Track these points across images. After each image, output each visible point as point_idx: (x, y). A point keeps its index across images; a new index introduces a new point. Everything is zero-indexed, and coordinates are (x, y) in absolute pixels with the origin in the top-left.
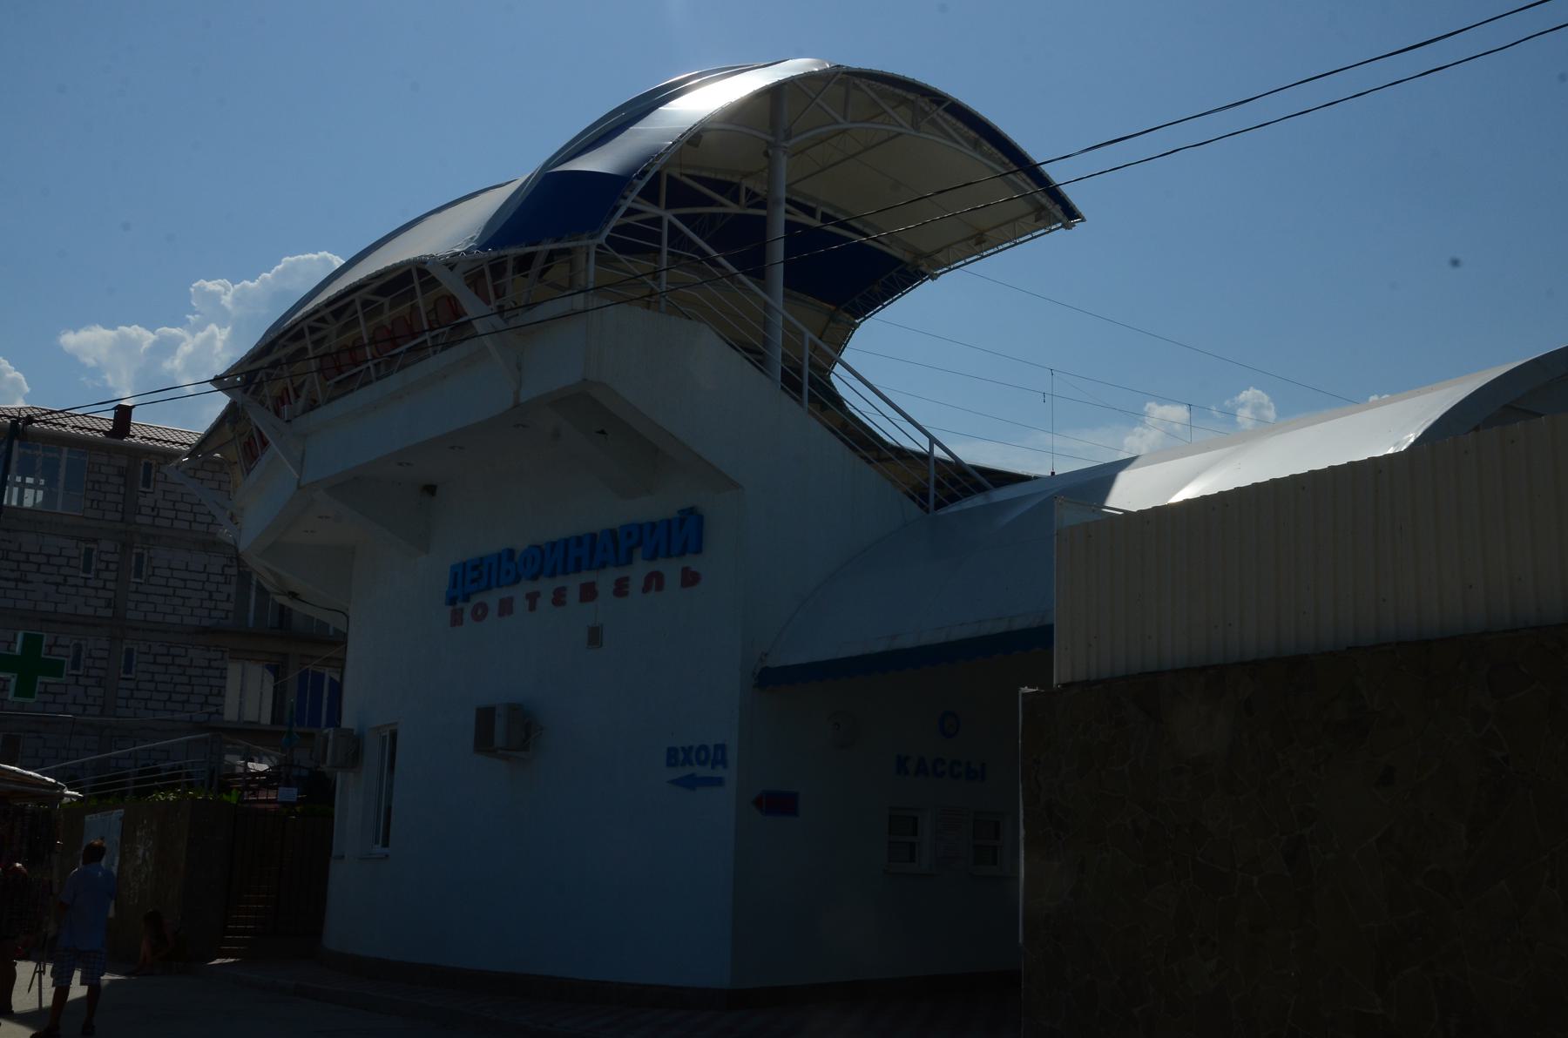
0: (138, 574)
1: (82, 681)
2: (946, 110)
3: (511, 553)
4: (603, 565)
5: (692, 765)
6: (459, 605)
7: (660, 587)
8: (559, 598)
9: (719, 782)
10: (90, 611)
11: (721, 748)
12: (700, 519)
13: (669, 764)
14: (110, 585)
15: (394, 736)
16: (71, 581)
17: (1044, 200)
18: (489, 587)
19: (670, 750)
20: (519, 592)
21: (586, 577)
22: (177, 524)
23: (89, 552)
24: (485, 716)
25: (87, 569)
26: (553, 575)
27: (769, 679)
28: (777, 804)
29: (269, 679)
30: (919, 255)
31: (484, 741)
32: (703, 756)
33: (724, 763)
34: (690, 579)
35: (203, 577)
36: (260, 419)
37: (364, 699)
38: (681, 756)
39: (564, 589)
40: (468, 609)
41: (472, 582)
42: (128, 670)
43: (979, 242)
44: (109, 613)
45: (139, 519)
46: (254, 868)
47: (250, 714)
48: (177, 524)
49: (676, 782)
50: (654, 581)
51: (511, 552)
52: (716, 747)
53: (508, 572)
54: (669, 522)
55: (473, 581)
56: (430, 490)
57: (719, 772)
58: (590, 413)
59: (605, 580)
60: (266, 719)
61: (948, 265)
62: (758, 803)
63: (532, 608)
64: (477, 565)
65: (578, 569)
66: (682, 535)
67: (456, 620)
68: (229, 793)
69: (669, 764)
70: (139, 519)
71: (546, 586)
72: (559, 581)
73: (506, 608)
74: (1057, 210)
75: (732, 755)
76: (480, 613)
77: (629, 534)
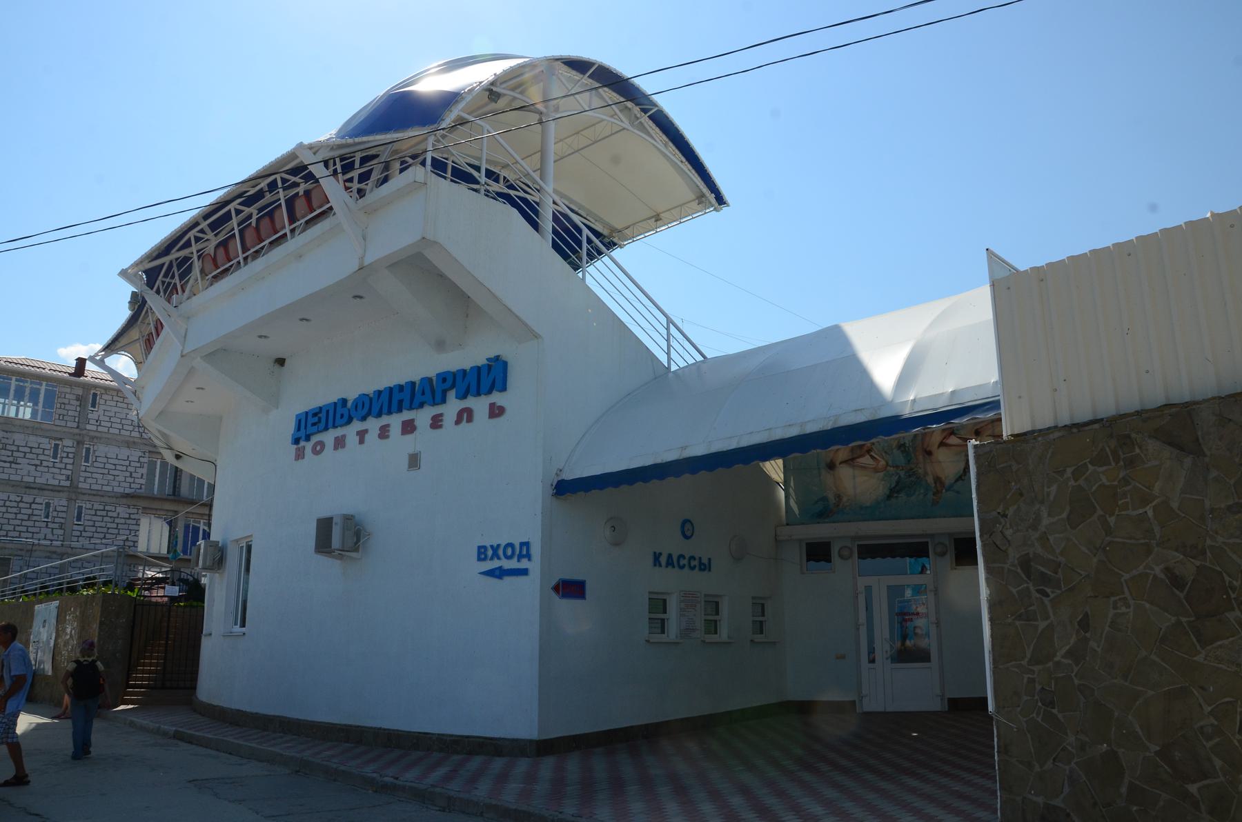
0: (87, 460)
1: (50, 525)
2: (650, 117)
3: (344, 402)
4: (421, 405)
5: (501, 561)
6: (302, 443)
7: (470, 420)
8: (384, 433)
9: (524, 572)
10: (56, 483)
11: (526, 544)
12: (505, 364)
13: (479, 559)
14: (69, 467)
15: (249, 548)
16: (45, 463)
17: (705, 190)
18: (326, 429)
19: (479, 548)
20: (351, 431)
21: (407, 415)
22: (112, 430)
23: (56, 446)
24: (324, 526)
25: (55, 457)
26: (379, 415)
27: (563, 489)
28: (571, 589)
29: (166, 528)
30: (614, 230)
31: (323, 543)
32: (509, 552)
33: (528, 556)
34: (496, 412)
35: (127, 463)
36: (155, 302)
37: (225, 523)
38: (490, 553)
39: (388, 426)
40: (309, 446)
41: (314, 424)
42: (79, 519)
43: (657, 219)
44: (68, 483)
45: (88, 427)
46: (147, 645)
47: (154, 550)
48: (112, 430)
49: (490, 573)
50: (466, 415)
51: (344, 401)
52: (522, 544)
53: (342, 416)
54: (479, 369)
55: (314, 424)
56: (281, 362)
57: (524, 564)
58: (420, 267)
59: (423, 417)
60: (164, 551)
61: (632, 237)
62: (556, 589)
63: (362, 441)
64: (317, 413)
65: (400, 410)
66: (490, 378)
67: (300, 455)
68: (132, 591)
69: (479, 559)
70: (88, 427)
71: (373, 425)
72: (385, 420)
73: (340, 443)
74: (712, 197)
75: (536, 550)
76: (319, 449)
77: (444, 380)
